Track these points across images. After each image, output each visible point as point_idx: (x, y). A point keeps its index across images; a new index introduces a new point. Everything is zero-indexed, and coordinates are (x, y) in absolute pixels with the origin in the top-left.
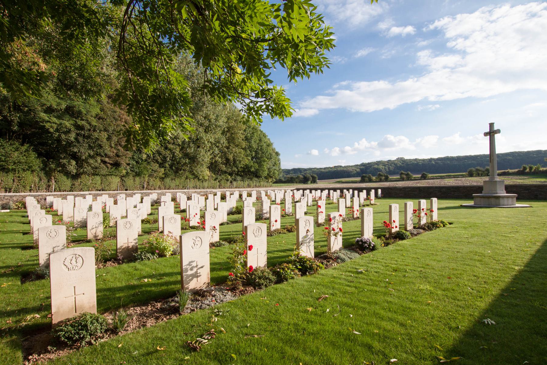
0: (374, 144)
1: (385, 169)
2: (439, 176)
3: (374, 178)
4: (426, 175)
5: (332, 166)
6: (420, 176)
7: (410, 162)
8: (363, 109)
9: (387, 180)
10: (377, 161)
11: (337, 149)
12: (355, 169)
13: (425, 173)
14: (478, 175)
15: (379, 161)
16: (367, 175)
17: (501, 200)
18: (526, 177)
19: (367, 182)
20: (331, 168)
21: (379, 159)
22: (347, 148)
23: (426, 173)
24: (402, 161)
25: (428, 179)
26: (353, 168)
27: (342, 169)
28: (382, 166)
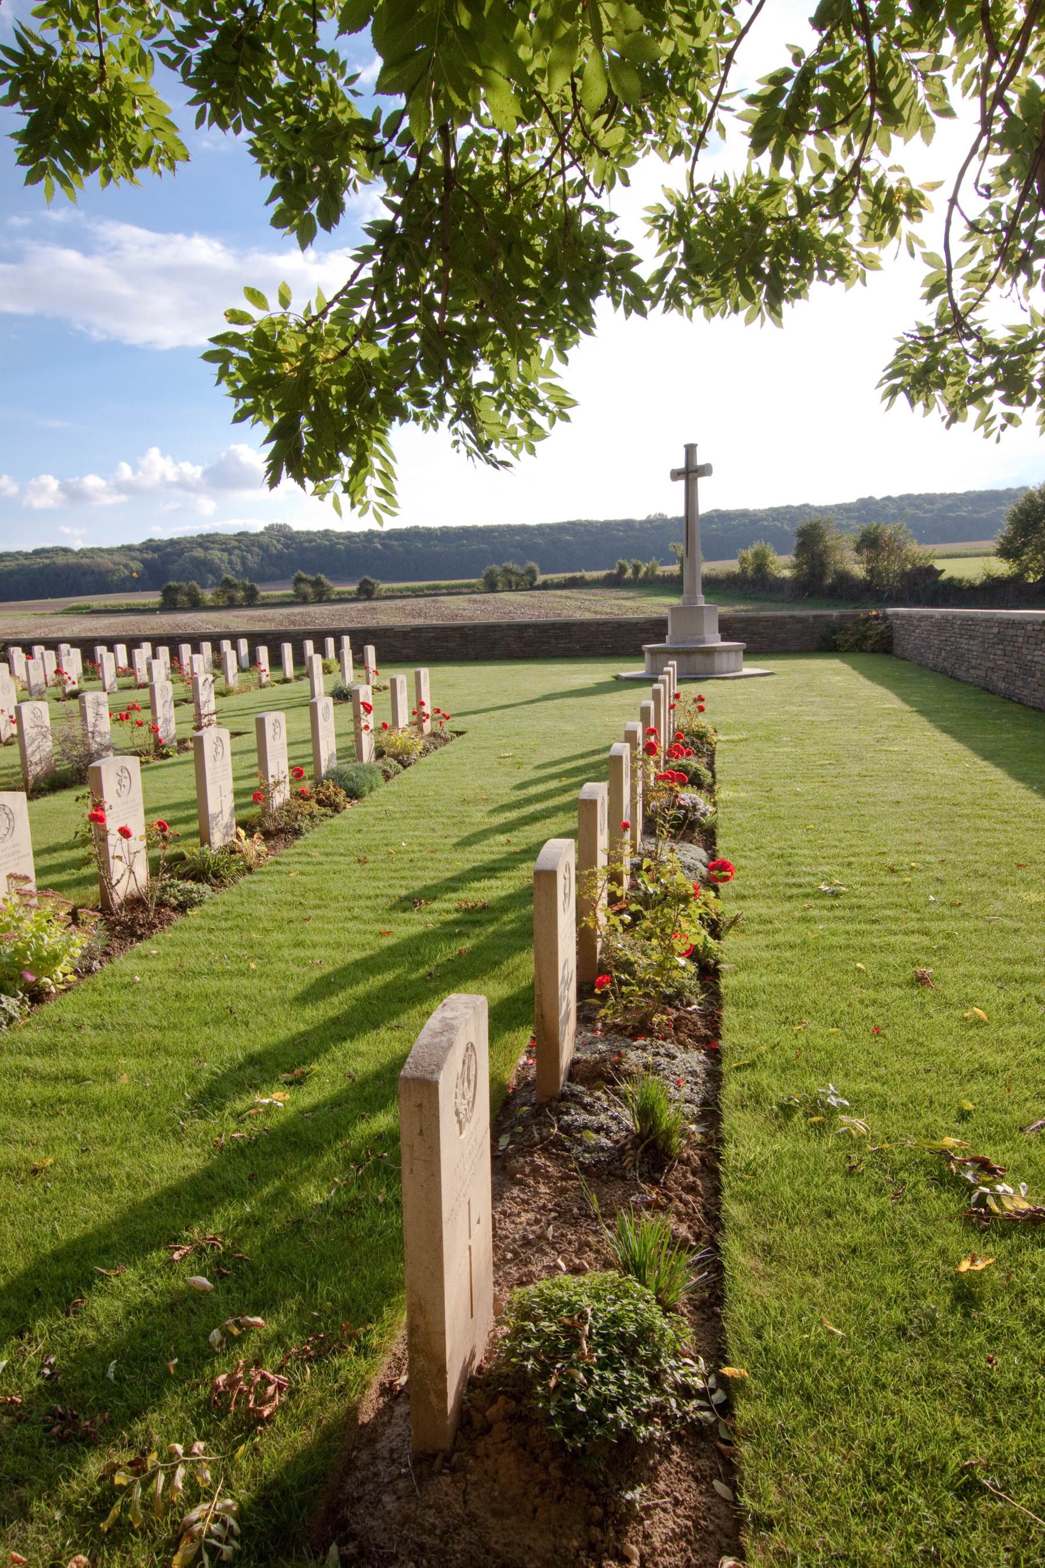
0: (193, 471)
1: (230, 562)
2: (408, 589)
3: (208, 595)
4: (372, 585)
5: (29, 547)
6: (354, 588)
7: (310, 541)
8: (138, 333)
9: (251, 600)
10: (201, 536)
11: (52, 483)
12: (124, 560)
13: (368, 578)
14: (510, 587)
15: (209, 536)
16: (183, 584)
17: (716, 657)
18: (631, 594)
19: (184, 610)
20: (27, 556)
21: (206, 529)
22: (93, 482)
23: (372, 580)
24: (285, 536)
25: (377, 599)
26: (116, 558)
27: (72, 560)
28: (219, 554)
